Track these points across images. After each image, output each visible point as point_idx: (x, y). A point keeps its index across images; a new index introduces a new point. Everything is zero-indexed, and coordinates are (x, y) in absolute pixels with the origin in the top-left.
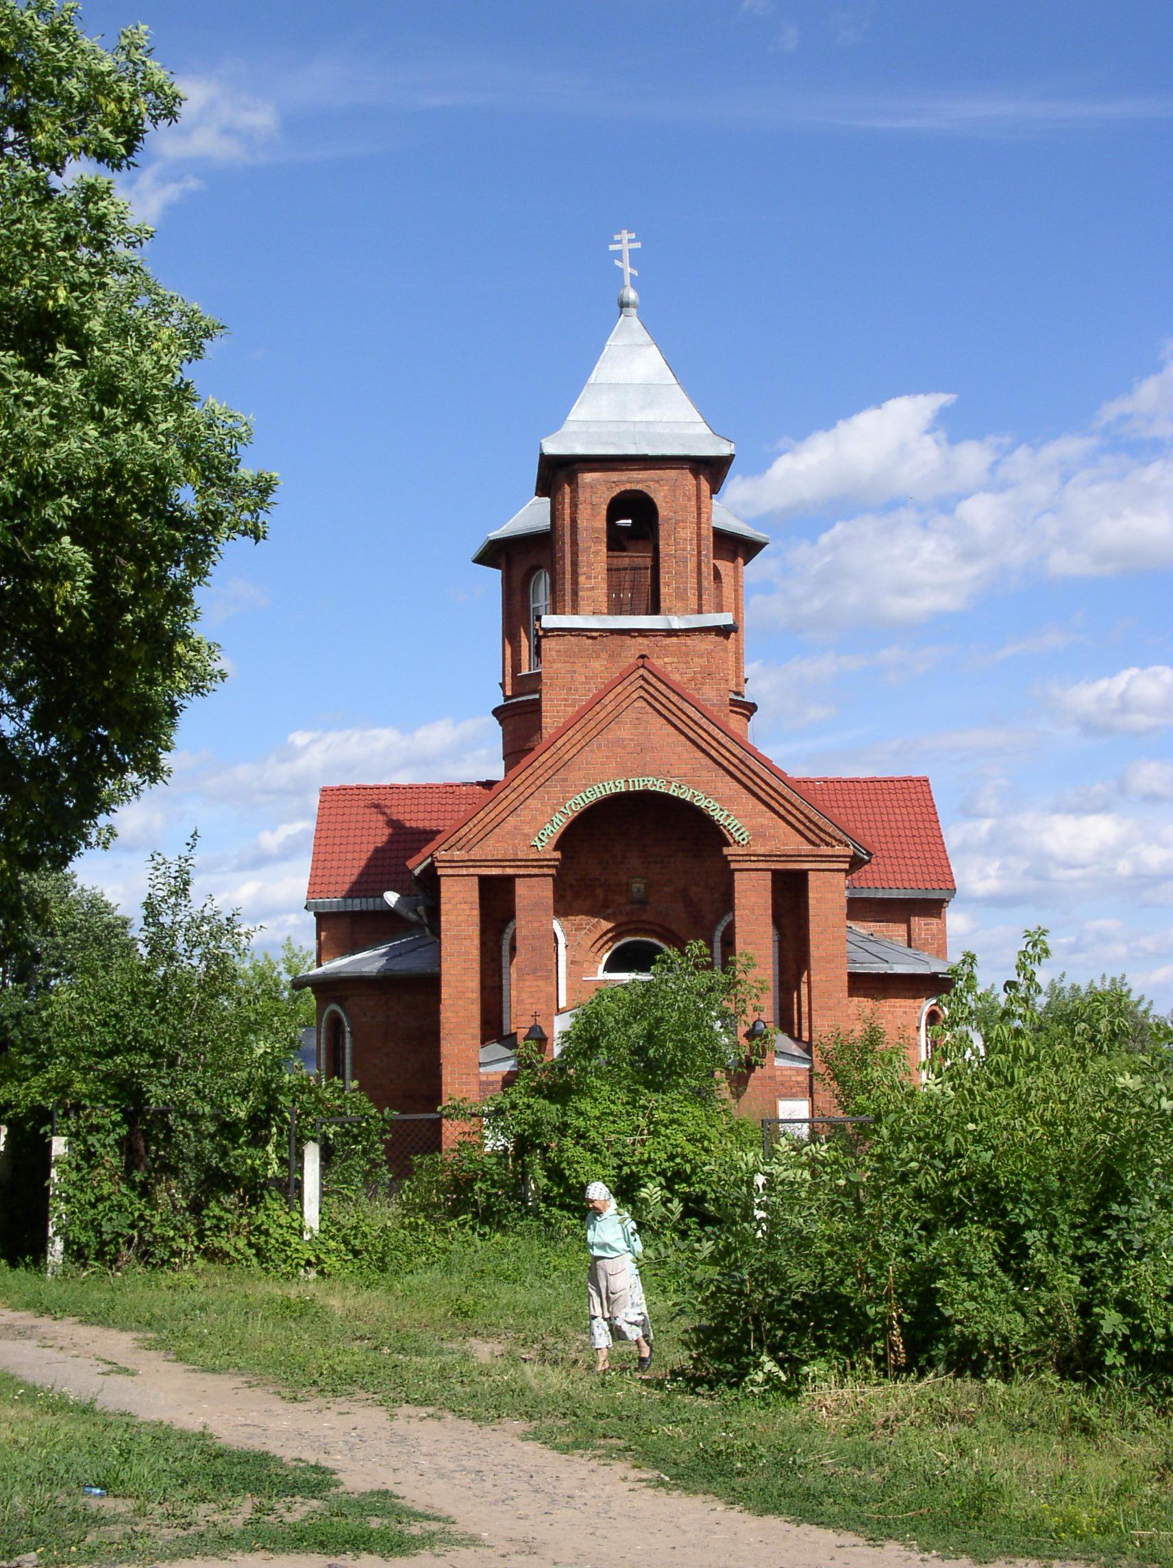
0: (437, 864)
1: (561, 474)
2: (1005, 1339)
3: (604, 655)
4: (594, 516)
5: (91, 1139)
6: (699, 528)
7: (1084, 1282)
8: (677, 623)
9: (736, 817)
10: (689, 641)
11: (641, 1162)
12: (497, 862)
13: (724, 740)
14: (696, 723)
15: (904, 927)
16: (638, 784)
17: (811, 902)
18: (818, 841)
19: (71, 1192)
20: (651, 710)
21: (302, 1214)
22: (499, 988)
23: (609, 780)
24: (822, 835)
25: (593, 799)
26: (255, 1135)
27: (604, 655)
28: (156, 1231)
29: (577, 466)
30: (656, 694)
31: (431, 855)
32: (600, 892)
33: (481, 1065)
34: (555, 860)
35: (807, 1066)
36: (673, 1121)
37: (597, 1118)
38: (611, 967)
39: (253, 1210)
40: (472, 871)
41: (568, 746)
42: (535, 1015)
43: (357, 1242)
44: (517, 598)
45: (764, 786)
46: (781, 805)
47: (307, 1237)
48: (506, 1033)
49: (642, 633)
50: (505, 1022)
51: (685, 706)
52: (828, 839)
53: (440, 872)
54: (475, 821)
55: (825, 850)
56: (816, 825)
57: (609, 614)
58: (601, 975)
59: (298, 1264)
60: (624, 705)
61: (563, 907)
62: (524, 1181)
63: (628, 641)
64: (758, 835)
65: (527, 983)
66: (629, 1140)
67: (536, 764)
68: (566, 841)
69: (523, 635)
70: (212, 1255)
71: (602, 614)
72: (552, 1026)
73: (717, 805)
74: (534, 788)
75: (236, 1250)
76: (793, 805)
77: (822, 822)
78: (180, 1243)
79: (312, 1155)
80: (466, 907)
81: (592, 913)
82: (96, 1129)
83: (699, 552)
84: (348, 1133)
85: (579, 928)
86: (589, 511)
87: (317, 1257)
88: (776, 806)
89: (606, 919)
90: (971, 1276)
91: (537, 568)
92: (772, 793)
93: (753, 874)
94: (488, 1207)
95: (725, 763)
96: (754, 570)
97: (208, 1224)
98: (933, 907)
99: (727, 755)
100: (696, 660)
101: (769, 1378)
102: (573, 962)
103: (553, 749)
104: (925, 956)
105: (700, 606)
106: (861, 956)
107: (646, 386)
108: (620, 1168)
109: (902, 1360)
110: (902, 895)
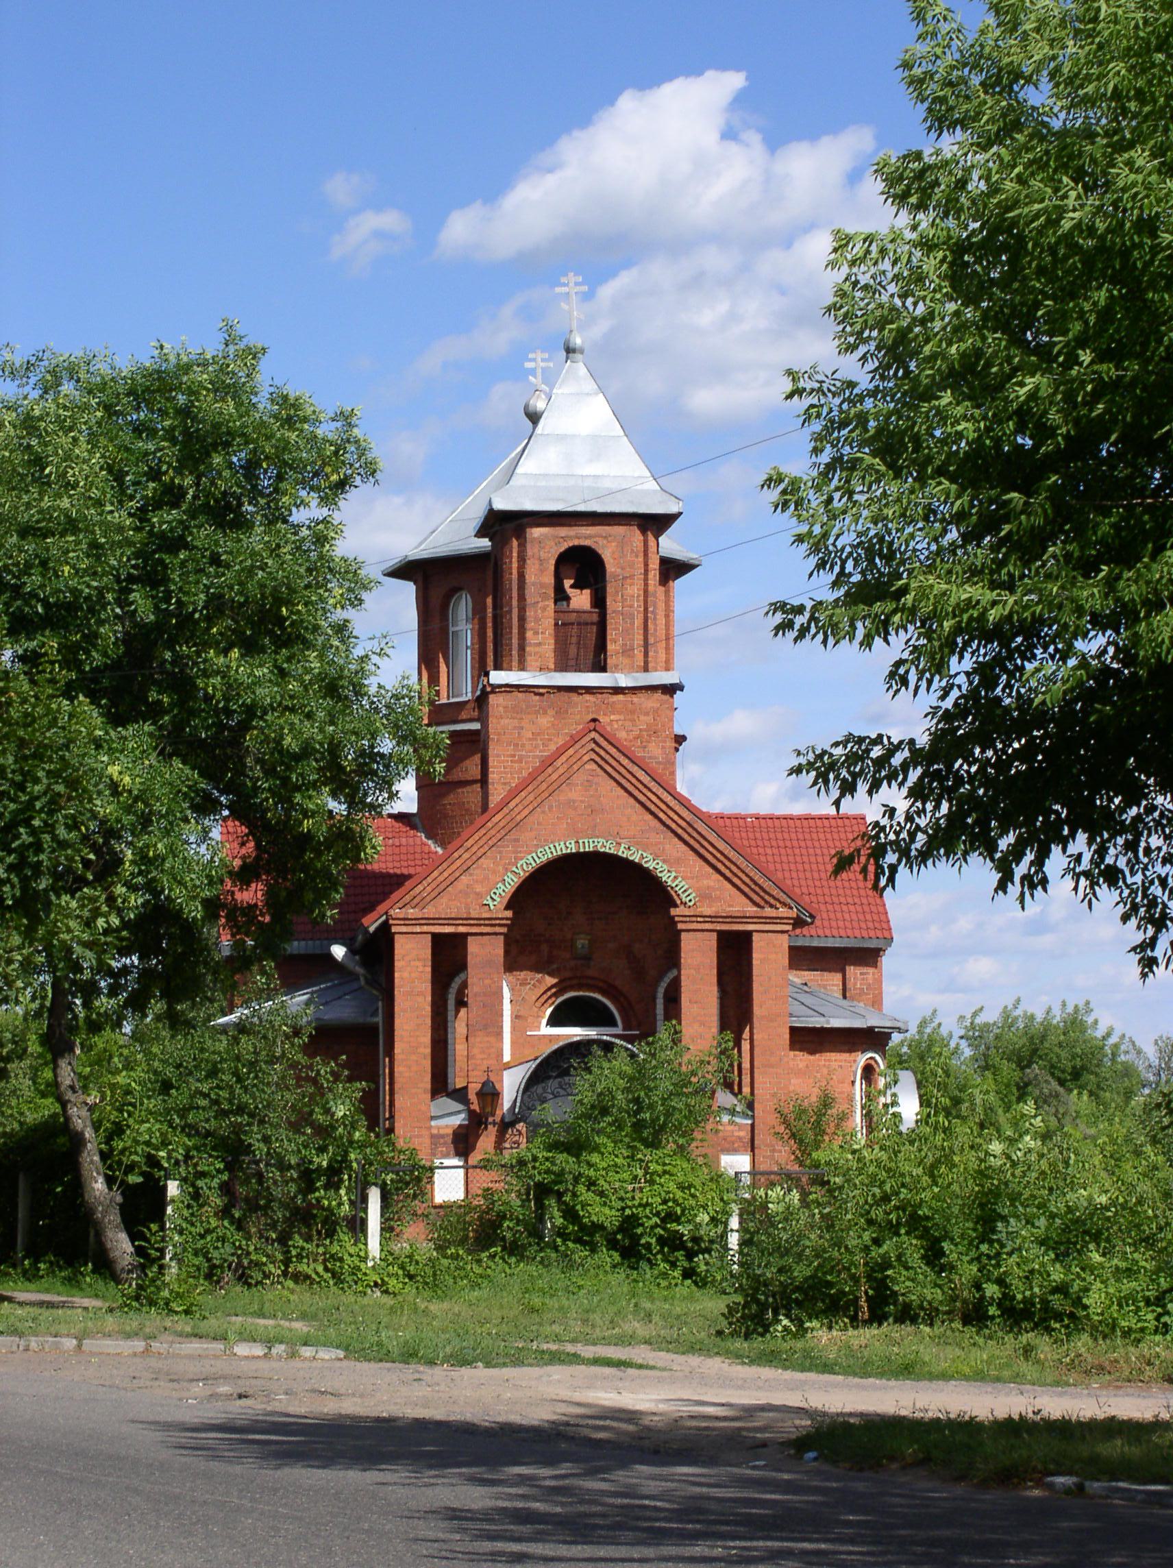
0: (391, 922)
1: (509, 526)
2: (930, 1303)
3: (551, 712)
4: (542, 571)
5: (200, 1183)
6: (646, 584)
7: (979, 1270)
8: (624, 681)
9: (683, 879)
10: (635, 699)
11: (640, 1205)
12: (450, 921)
13: (672, 803)
14: (645, 786)
15: (839, 976)
16: (588, 845)
17: (755, 962)
18: (762, 903)
19: (184, 1225)
20: (602, 773)
21: (366, 1244)
22: (445, 1042)
23: (559, 841)
24: (767, 897)
25: (544, 859)
26: (329, 1180)
27: (551, 712)
28: (254, 1257)
29: (525, 520)
30: (607, 757)
31: (386, 913)
32: (545, 948)
33: (433, 1118)
34: (507, 919)
35: (750, 1122)
36: (665, 1172)
37: (604, 1169)
38: (554, 1021)
39: (327, 1242)
40: (425, 929)
41: (520, 807)
42: (488, 1070)
43: (412, 1268)
44: (435, 625)
45: (711, 849)
46: (727, 867)
47: (370, 1264)
48: (451, 1087)
49: (589, 690)
50: (450, 1075)
51: (635, 769)
52: (772, 901)
53: (394, 929)
54: (429, 879)
55: (768, 911)
56: (761, 888)
57: (555, 671)
58: (546, 1030)
59: (368, 1285)
60: (575, 767)
61: (511, 965)
62: (541, 1219)
63: (575, 697)
64: (704, 896)
65: (478, 1039)
66: (630, 1187)
67: (490, 824)
68: (516, 901)
69: (441, 660)
70: (298, 1278)
71: (549, 670)
72: (502, 1081)
73: (665, 867)
74: (486, 848)
75: (317, 1273)
76: (738, 867)
77: (767, 885)
78: (271, 1268)
79: (374, 1196)
80: (417, 963)
81: (537, 968)
82: (203, 1175)
83: (646, 609)
84: (400, 1181)
85: (524, 983)
86: (537, 566)
87: (382, 1279)
88: (722, 868)
89: (551, 974)
90: (907, 1268)
91: (455, 590)
92: (719, 855)
93: (699, 934)
94: (514, 1242)
95: (674, 826)
96: (680, 585)
97: (294, 1253)
98: (869, 956)
99: (676, 817)
100: (642, 718)
101: (785, 1328)
102: (517, 1017)
103: (506, 810)
104: (860, 1006)
105: (646, 663)
106: (797, 1008)
107: (594, 438)
108: (623, 1209)
109: (866, 1316)
110: (838, 943)
